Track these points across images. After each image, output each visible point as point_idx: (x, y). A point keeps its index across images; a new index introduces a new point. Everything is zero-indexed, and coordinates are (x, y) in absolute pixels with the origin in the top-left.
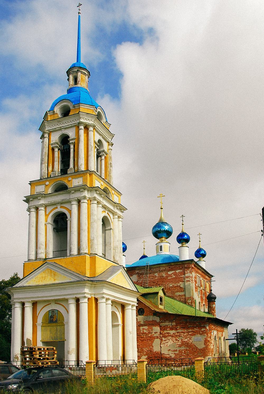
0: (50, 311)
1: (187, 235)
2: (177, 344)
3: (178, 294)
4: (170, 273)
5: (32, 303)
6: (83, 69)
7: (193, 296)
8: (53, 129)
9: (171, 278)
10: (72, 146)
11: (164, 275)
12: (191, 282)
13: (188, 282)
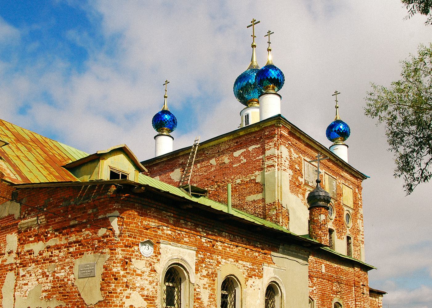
2: (43, 289)
3: (250, 198)
4: (236, 154)
7: (281, 201)
9: (240, 165)
12: (276, 167)
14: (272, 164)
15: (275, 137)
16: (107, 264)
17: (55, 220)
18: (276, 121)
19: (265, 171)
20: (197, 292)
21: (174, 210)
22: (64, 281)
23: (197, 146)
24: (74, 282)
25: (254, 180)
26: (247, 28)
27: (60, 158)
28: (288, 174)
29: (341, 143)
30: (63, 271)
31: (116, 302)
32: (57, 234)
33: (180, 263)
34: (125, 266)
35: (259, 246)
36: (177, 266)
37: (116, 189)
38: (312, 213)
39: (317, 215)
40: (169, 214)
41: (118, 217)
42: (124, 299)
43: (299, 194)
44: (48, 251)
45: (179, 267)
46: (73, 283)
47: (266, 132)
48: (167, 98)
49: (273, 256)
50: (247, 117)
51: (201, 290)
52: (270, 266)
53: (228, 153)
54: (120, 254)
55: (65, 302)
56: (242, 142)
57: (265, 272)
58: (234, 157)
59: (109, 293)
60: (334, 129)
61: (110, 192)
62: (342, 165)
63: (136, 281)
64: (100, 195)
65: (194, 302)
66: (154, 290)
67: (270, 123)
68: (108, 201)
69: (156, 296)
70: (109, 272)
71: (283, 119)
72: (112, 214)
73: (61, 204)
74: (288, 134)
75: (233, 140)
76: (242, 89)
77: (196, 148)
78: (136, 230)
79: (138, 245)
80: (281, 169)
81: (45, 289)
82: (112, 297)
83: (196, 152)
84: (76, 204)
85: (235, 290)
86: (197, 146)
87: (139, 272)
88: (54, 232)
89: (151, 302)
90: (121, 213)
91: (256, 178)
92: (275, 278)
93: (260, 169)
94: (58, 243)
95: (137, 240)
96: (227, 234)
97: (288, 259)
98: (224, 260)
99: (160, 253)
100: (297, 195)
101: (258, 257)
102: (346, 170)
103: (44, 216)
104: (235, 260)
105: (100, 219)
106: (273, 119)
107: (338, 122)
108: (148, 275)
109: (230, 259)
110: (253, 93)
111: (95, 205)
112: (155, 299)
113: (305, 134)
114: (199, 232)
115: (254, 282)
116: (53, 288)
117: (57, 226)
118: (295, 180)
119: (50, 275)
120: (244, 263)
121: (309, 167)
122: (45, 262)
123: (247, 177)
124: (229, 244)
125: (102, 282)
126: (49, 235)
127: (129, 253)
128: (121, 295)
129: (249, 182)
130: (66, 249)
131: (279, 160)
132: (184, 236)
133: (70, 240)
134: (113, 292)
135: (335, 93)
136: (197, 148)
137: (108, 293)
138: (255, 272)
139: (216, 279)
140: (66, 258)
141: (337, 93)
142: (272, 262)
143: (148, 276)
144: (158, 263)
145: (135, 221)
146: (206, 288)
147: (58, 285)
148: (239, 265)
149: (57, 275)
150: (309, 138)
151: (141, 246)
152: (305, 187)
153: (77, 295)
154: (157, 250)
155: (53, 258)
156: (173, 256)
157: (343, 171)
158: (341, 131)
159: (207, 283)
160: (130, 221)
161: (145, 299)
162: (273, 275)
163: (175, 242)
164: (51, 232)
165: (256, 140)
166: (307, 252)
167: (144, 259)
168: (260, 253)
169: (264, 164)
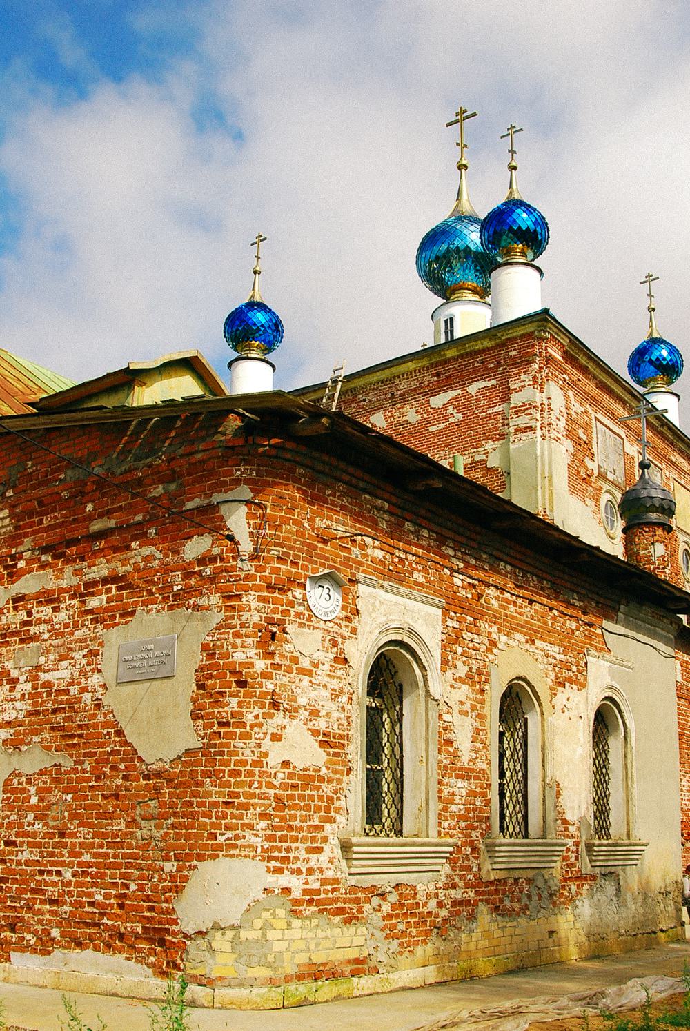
1: (528, 208)
4: (437, 401)
7: (551, 511)
12: (539, 432)
13: (523, 436)
14: (528, 425)
15: (533, 362)
16: (215, 638)
17: (43, 519)
18: (536, 324)
19: (511, 441)
20: (446, 724)
21: (391, 493)
22: (68, 694)
23: (340, 381)
24: (102, 695)
25: (483, 462)
26: (447, 126)
27: (20, 387)
28: (565, 449)
29: (663, 390)
30: (65, 664)
31: (241, 751)
32: (48, 561)
33: (404, 640)
34: (269, 645)
35: (577, 604)
36: (396, 648)
37: (242, 424)
38: (634, 538)
39: (646, 545)
40: (379, 502)
41: (248, 503)
42: (267, 744)
43: (588, 499)
44: (16, 609)
45: (402, 651)
46: (101, 700)
47: (511, 351)
48: (259, 274)
49: (607, 630)
50: (450, 322)
51: (454, 718)
52: (601, 657)
53: (415, 398)
54: (254, 609)
55: (71, 755)
56: (451, 373)
57: (591, 672)
58: (431, 408)
59: (221, 724)
60: (647, 358)
61: (223, 433)
62: (672, 438)
63: (299, 691)
64: (192, 442)
65: (440, 751)
66: (342, 716)
67: (520, 331)
68: (216, 460)
69: (348, 734)
70: (221, 662)
71: (553, 321)
72: (229, 496)
73: (62, 476)
74: (563, 357)
75: (428, 369)
76: (437, 259)
77: (336, 386)
78: (298, 543)
79: (303, 586)
80: (550, 437)
81: (7, 719)
82: (232, 739)
83: (336, 396)
84: (110, 471)
85: (527, 718)
86: (340, 383)
87: (305, 663)
88: (37, 553)
89: (337, 750)
90: (256, 492)
91: (487, 457)
92: (613, 688)
93: (498, 436)
94: (50, 585)
95: (300, 571)
96: (509, 568)
97: (637, 640)
98: (504, 638)
99: (358, 611)
100: (583, 500)
101: (577, 633)
102: (679, 450)
103: (7, 511)
104: (528, 638)
105: (189, 510)
106: (530, 319)
107: (655, 342)
108: (329, 673)
109: (518, 636)
110: (464, 271)
111: (174, 472)
112: (345, 742)
113: (598, 360)
114: (447, 557)
115: (568, 699)
116: (30, 715)
117: (47, 538)
118: (578, 465)
119: (22, 679)
120: (548, 647)
121: (608, 436)
122: (7, 639)
123: (465, 454)
124: (514, 595)
125: (197, 694)
126: (21, 564)
127: (281, 608)
128: (256, 729)
129: (469, 468)
130: (75, 602)
131: (545, 414)
132: (414, 565)
133: (88, 576)
134: (232, 721)
135: (647, 279)
136: (339, 388)
137: (216, 725)
138: (570, 673)
139: (487, 687)
140: (76, 625)
141: (651, 278)
142: (604, 646)
143: (329, 676)
144: (352, 638)
145: (296, 517)
146: (466, 713)
147: (50, 705)
148: (536, 651)
149: (44, 677)
150: (607, 368)
151: (311, 589)
152: (600, 483)
153: (113, 735)
154: (350, 601)
155: (33, 630)
156: (389, 621)
157: (673, 450)
158: (665, 363)
159: (468, 699)
160: (283, 514)
161: (322, 743)
162: (608, 681)
163: (392, 582)
164: (27, 555)
165: (487, 369)
166: (674, 625)
167: (317, 625)
168: (580, 622)
169: (508, 424)
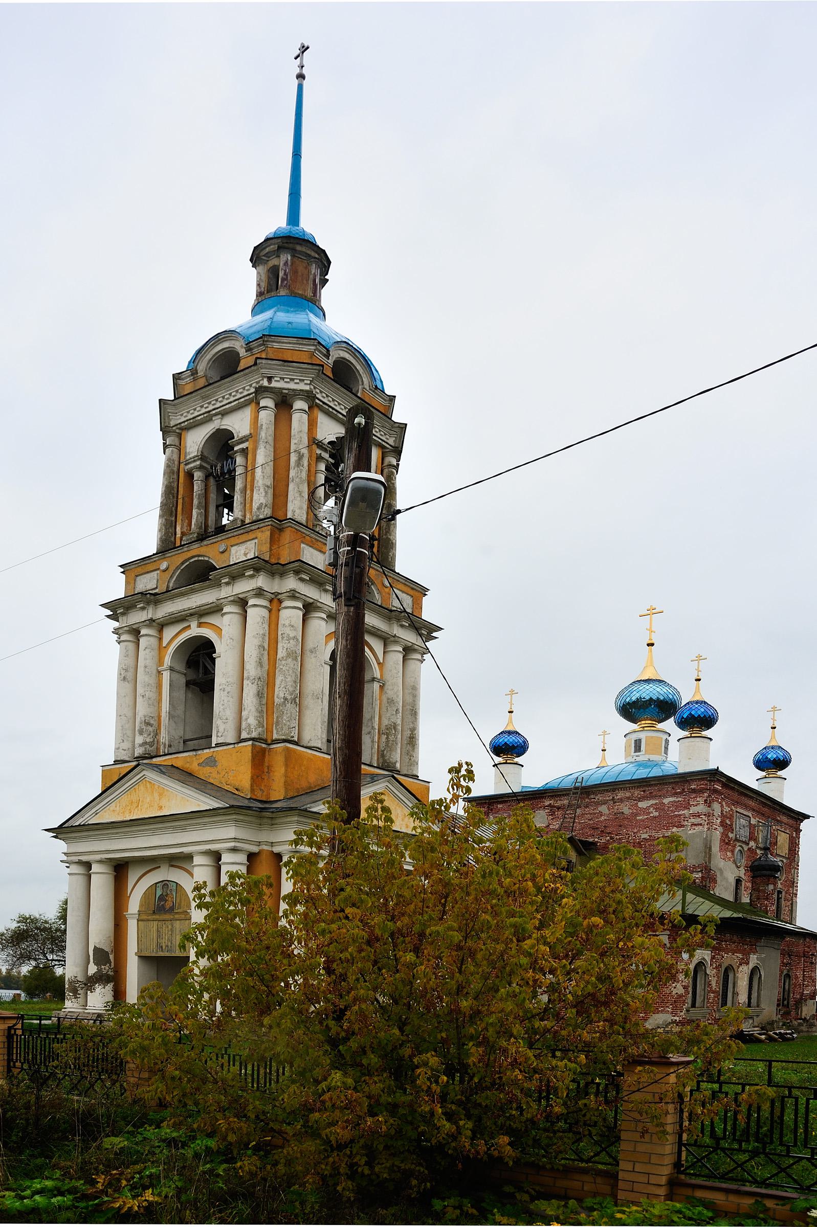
0: (156, 883)
4: (643, 805)
5: (115, 864)
6: (297, 243)
7: (710, 863)
8: (187, 420)
10: (239, 460)
11: (626, 809)
13: (697, 828)
